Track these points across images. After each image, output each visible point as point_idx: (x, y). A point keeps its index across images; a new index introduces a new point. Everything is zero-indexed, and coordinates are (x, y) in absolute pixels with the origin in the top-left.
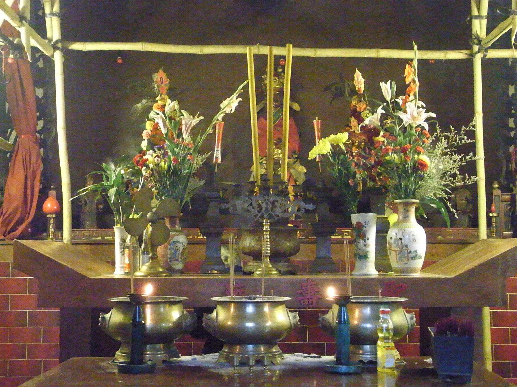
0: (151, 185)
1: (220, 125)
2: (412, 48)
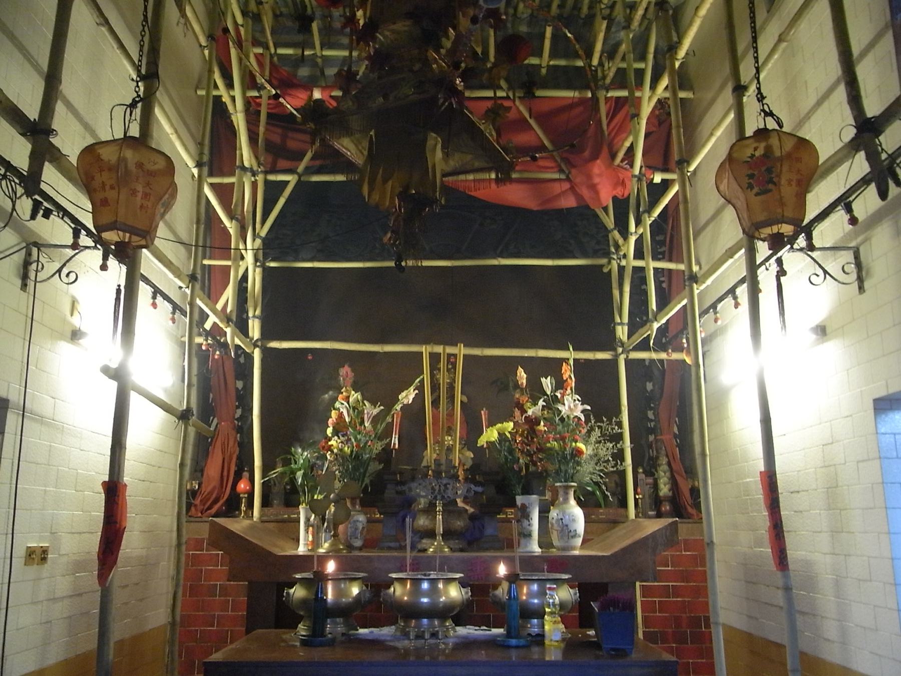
1: (398, 415)
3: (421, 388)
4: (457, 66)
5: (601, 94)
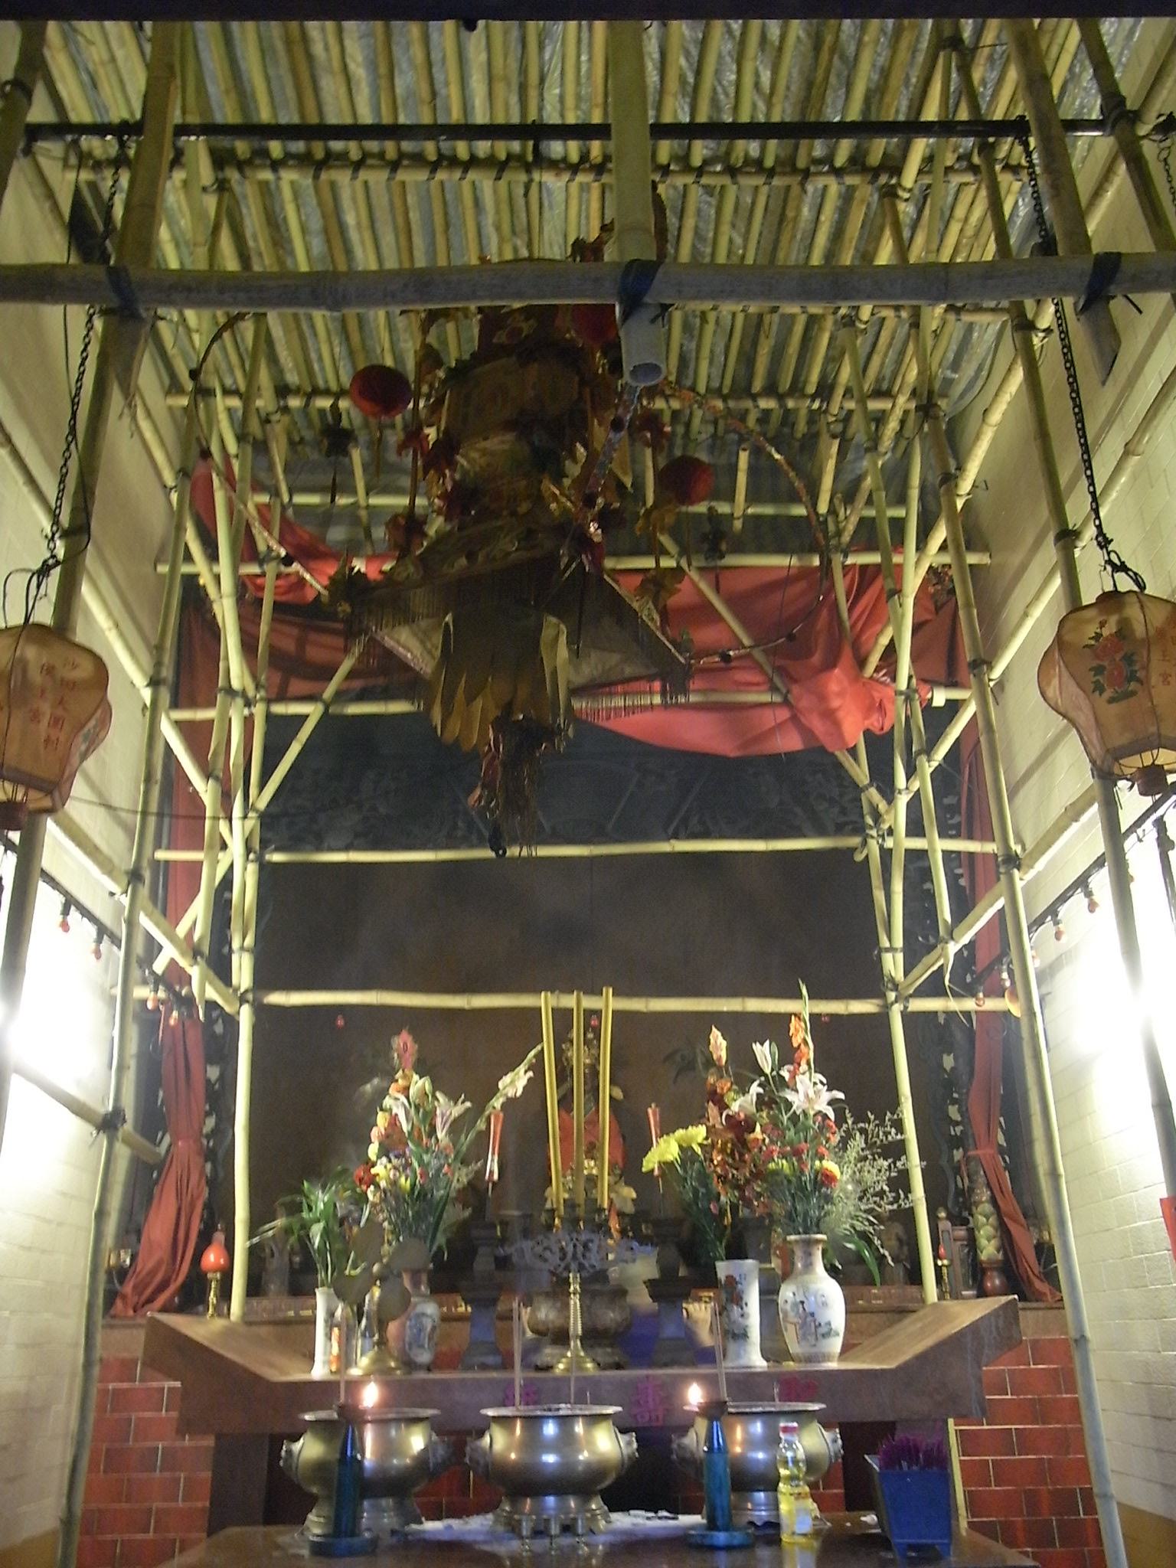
0: (381, 1217)
1: (497, 1117)
2: (800, 996)
3: (538, 1067)
4: (590, 501)
5: (837, 559)
